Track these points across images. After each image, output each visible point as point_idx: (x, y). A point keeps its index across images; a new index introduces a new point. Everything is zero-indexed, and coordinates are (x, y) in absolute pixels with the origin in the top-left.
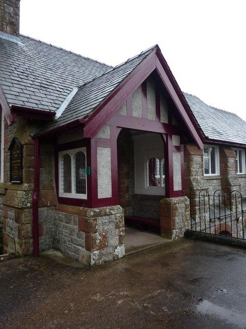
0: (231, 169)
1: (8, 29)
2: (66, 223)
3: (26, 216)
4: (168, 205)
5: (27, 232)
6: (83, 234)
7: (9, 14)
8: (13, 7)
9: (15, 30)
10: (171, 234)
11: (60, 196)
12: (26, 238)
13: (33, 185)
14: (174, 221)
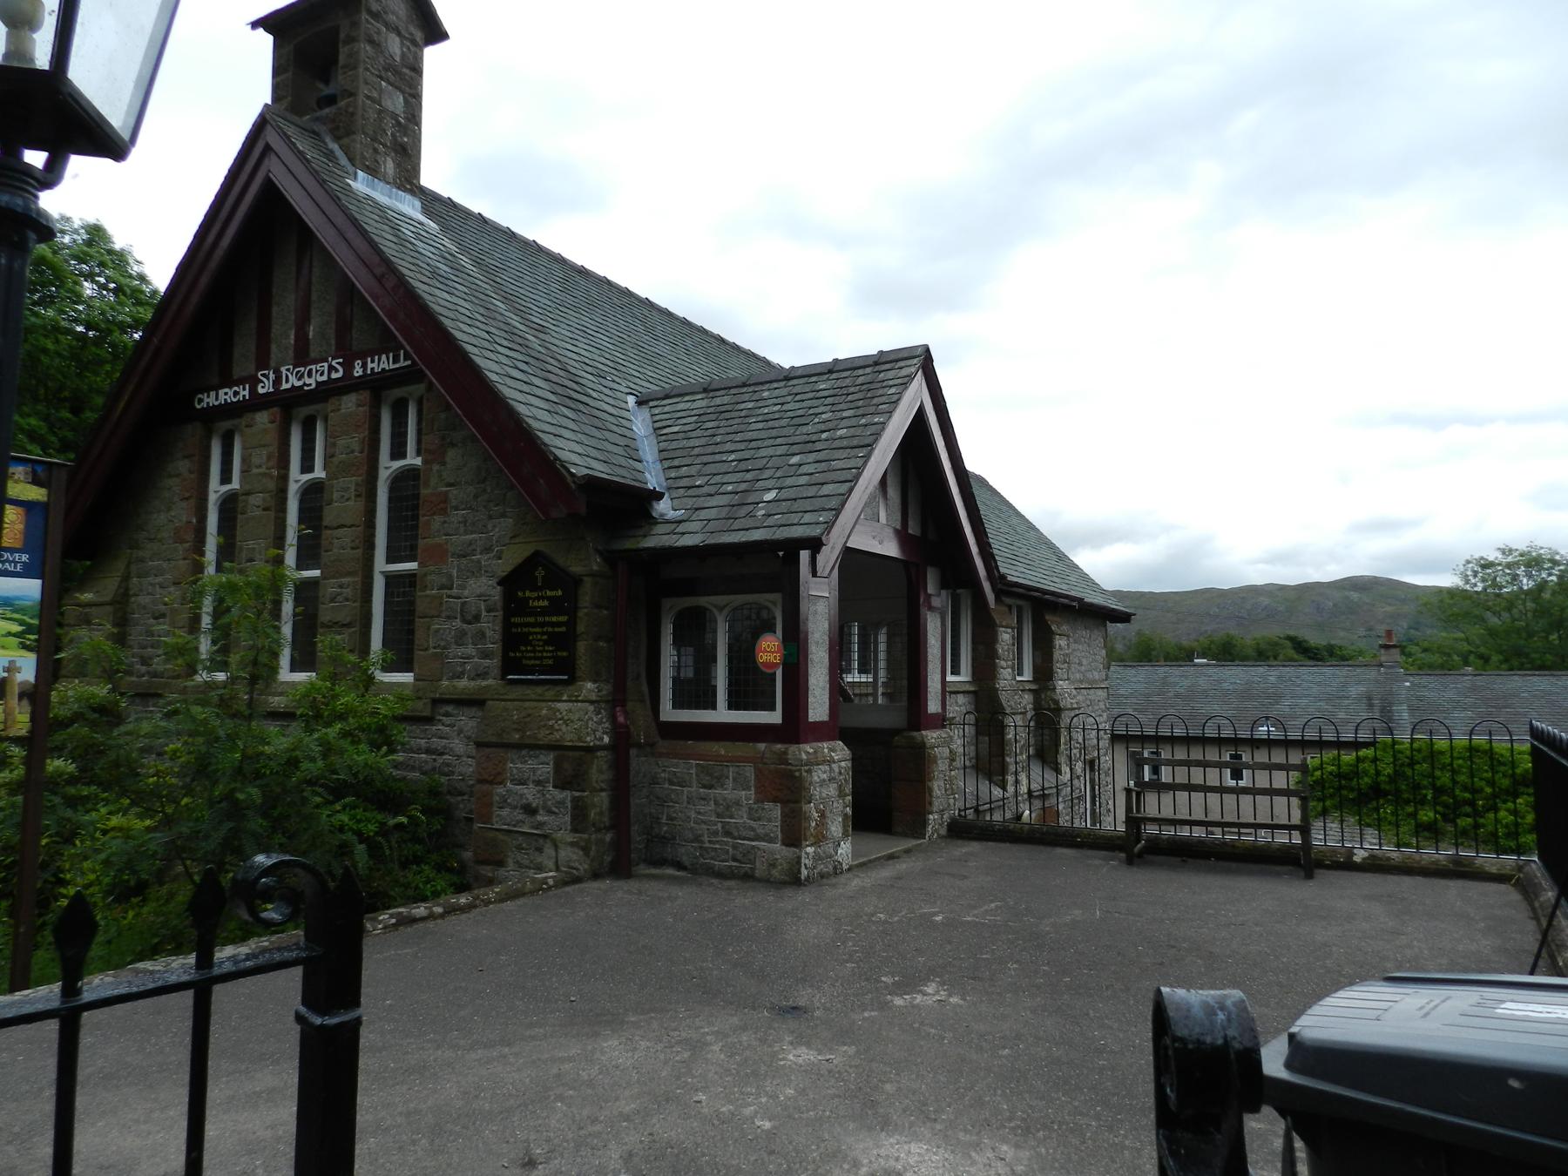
0: (1003, 663)
1: (389, 166)
2: (704, 787)
3: (601, 772)
4: (922, 747)
5: (601, 813)
6: (776, 811)
7: (395, 116)
8: (403, 92)
9: (408, 178)
10: (924, 823)
11: (664, 717)
12: (599, 830)
13: (607, 689)
14: (931, 790)
